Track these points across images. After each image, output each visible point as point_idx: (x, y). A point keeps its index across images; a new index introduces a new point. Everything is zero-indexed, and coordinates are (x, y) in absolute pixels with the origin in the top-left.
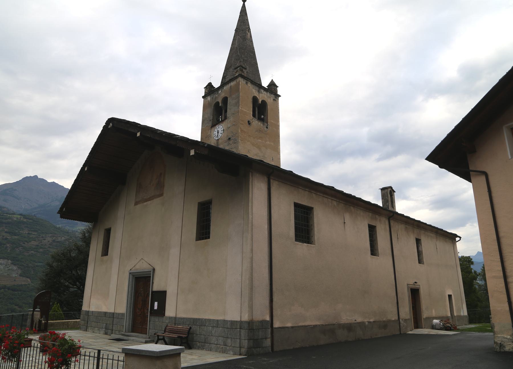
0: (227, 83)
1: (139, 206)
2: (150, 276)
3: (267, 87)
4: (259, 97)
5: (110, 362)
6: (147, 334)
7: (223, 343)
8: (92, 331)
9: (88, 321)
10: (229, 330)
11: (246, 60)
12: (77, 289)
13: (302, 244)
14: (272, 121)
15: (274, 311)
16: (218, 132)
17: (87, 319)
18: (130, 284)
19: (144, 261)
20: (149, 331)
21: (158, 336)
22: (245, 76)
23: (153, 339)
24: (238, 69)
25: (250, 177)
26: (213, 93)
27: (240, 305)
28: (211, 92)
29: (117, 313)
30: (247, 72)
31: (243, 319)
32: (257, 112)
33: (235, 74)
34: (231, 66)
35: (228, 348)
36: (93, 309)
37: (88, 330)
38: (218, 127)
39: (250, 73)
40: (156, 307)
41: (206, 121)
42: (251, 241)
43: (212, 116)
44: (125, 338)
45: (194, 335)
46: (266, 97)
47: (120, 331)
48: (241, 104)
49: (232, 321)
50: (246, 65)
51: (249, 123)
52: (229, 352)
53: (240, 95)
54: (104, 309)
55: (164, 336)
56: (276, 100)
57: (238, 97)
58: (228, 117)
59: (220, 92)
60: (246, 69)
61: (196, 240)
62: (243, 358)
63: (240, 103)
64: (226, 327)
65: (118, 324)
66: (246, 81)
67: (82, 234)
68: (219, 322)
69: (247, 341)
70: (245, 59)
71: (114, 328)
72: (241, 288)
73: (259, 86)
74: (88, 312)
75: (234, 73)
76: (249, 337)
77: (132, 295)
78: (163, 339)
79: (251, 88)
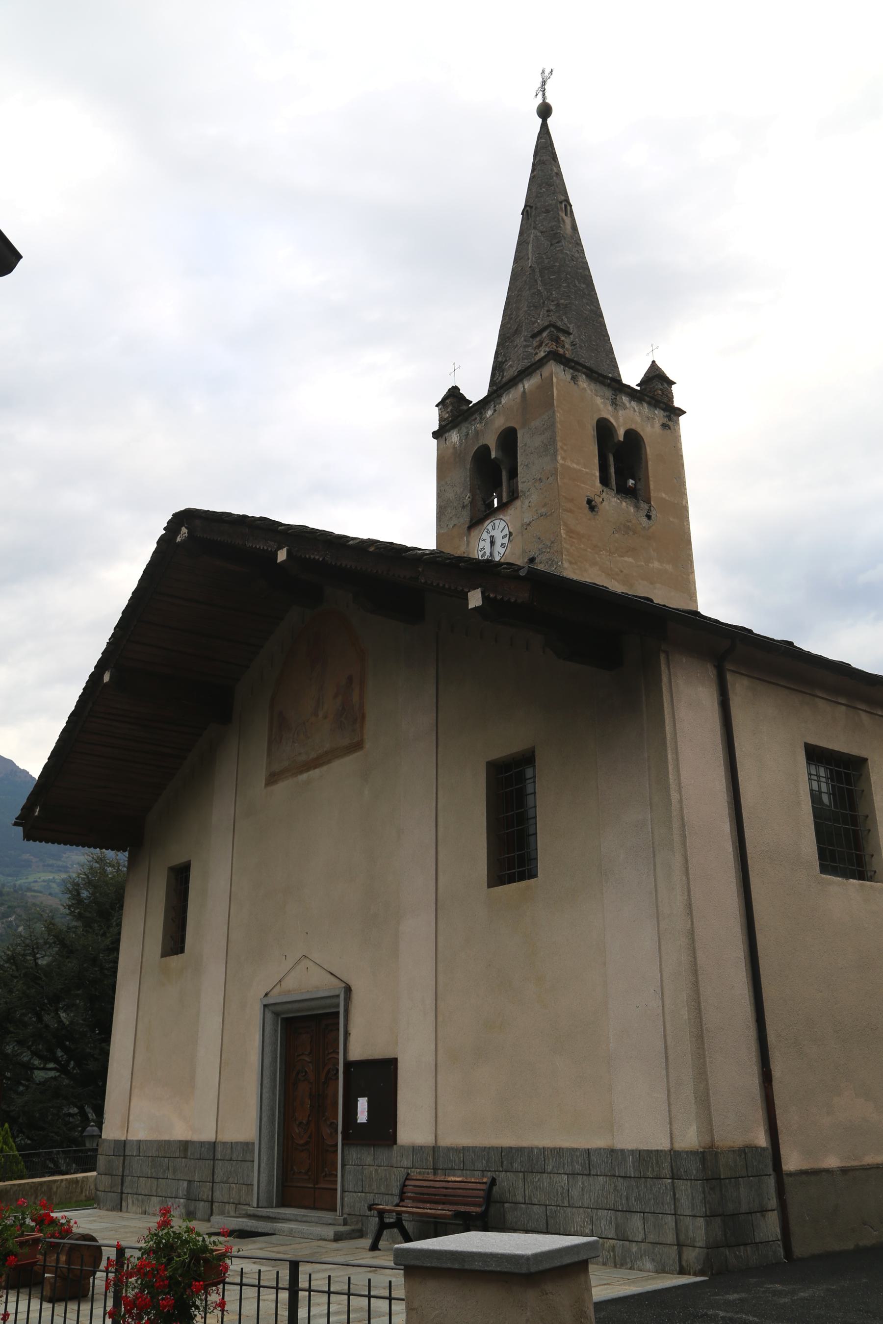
0: (511, 384)
1: (281, 787)
2: (338, 1013)
3: (637, 385)
4: (617, 419)
5: (268, 1296)
6: (336, 1211)
7: (613, 1231)
8: (139, 1210)
9: (123, 1176)
10: (633, 1183)
11: (566, 306)
12: (57, 1074)
13: (845, 880)
14: (664, 495)
15: (778, 1112)
16: (492, 543)
17: (121, 1169)
18: (267, 1041)
19: (310, 964)
20: (342, 1198)
21: (381, 1214)
22: (567, 355)
23: (359, 1226)
24: (545, 334)
25: (663, 666)
26: (466, 419)
27: (665, 1097)
28: (459, 416)
29: (224, 1143)
30: (573, 344)
31: (680, 1145)
32: (612, 470)
33: (536, 354)
34: (517, 329)
35: (634, 1248)
36: (139, 1132)
37: (124, 1208)
38: (490, 527)
39: (581, 347)
40: (362, 1116)
41: (449, 510)
42: (684, 878)
43: (470, 492)
44: (261, 1226)
45: (506, 1205)
46: (638, 419)
47: (239, 1204)
48: (562, 448)
49: (640, 1151)
50: (566, 320)
51: (591, 505)
52: (639, 1264)
53: (558, 420)
54: (179, 1132)
55: (399, 1214)
56: (672, 427)
57: (552, 425)
58: (522, 491)
59: (490, 413)
60: (567, 333)
61: (490, 886)
62: (704, 1281)
63: (559, 444)
64: (622, 1174)
65: (231, 1180)
66: (571, 371)
67: (71, 892)
68: (594, 1158)
69: (701, 1222)
70: (562, 301)
71: (217, 1194)
72: (665, 1036)
73: (614, 383)
74: (122, 1146)
75: (530, 350)
76: (707, 1206)
77: (274, 1080)
78: (398, 1224)
79: (589, 392)
